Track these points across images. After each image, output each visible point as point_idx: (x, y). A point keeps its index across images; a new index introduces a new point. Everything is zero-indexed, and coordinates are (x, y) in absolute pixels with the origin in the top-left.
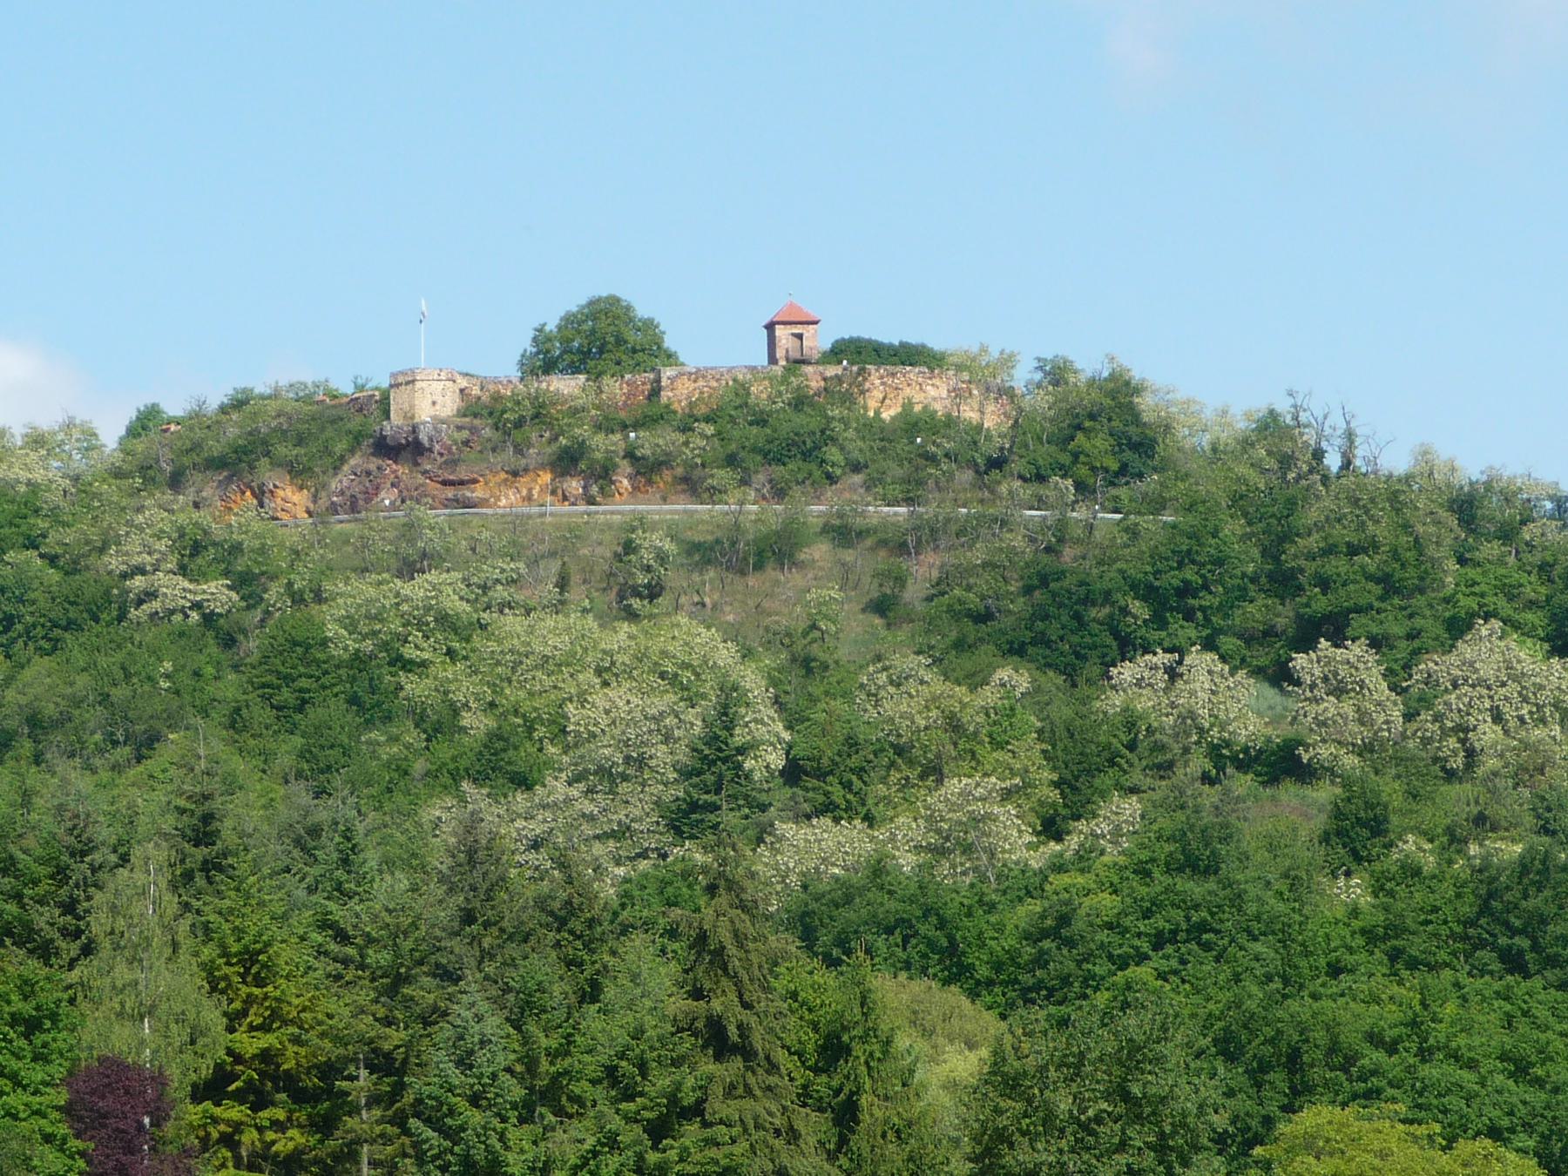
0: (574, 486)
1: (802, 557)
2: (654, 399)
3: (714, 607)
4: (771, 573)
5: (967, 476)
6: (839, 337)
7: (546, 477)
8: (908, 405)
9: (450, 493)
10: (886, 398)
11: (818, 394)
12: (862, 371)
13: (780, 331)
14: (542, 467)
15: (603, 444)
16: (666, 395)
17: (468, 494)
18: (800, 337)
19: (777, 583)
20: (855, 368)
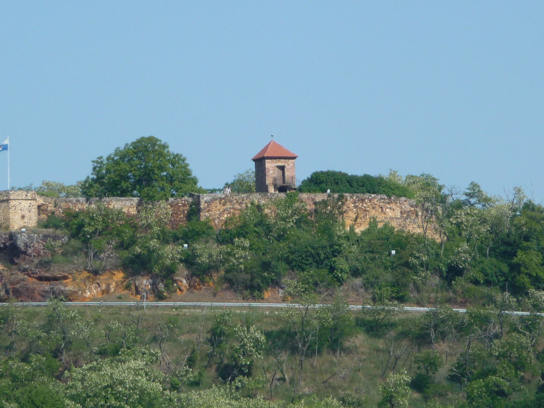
0: (145, 282)
1: (347, 344)
2: (195, 218)
3: (292, 381)
4: (327, 356)
5: (436, 280)
6: (152, 135)
7: (119, 275)
8: (374, 223)
9: (46, 286)
10: (358, 217)
11: (310, 214)
12: (341, 198)
13: (270, 165)
14: (116, 267)
15: (171, 252)
16: (204, 216)
17: (62, 288)
18: (282, 168)
19: (332, 364)
20: (336, 195)
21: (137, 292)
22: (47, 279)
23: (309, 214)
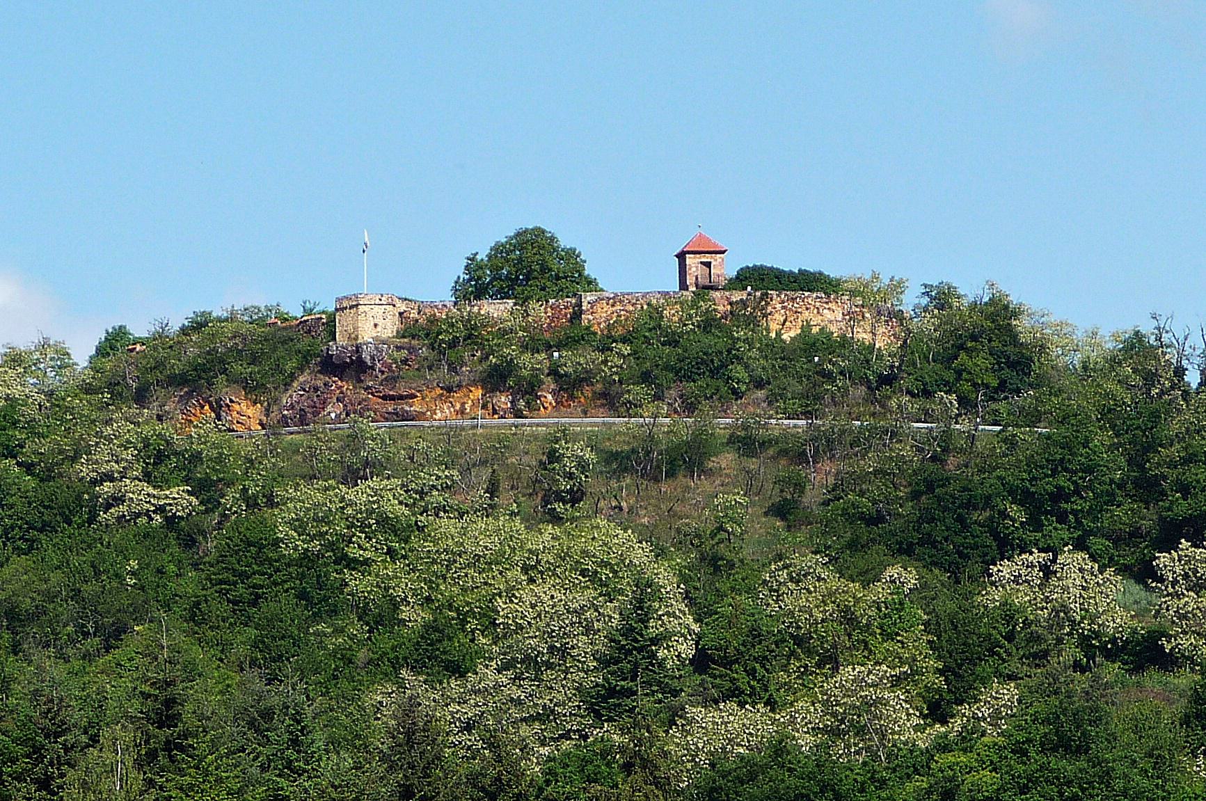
0: (503, 400)
5: (862, 391)
7: (478, 393)
8: (807, 327)
10: (785, 321)
13: (690, 260)
14: (474, 383)
15: (529, 362)
18: (708, 265)
20: (758, 294)
21: (495, 412)
22: (392, 398)
23: (722, 317)
